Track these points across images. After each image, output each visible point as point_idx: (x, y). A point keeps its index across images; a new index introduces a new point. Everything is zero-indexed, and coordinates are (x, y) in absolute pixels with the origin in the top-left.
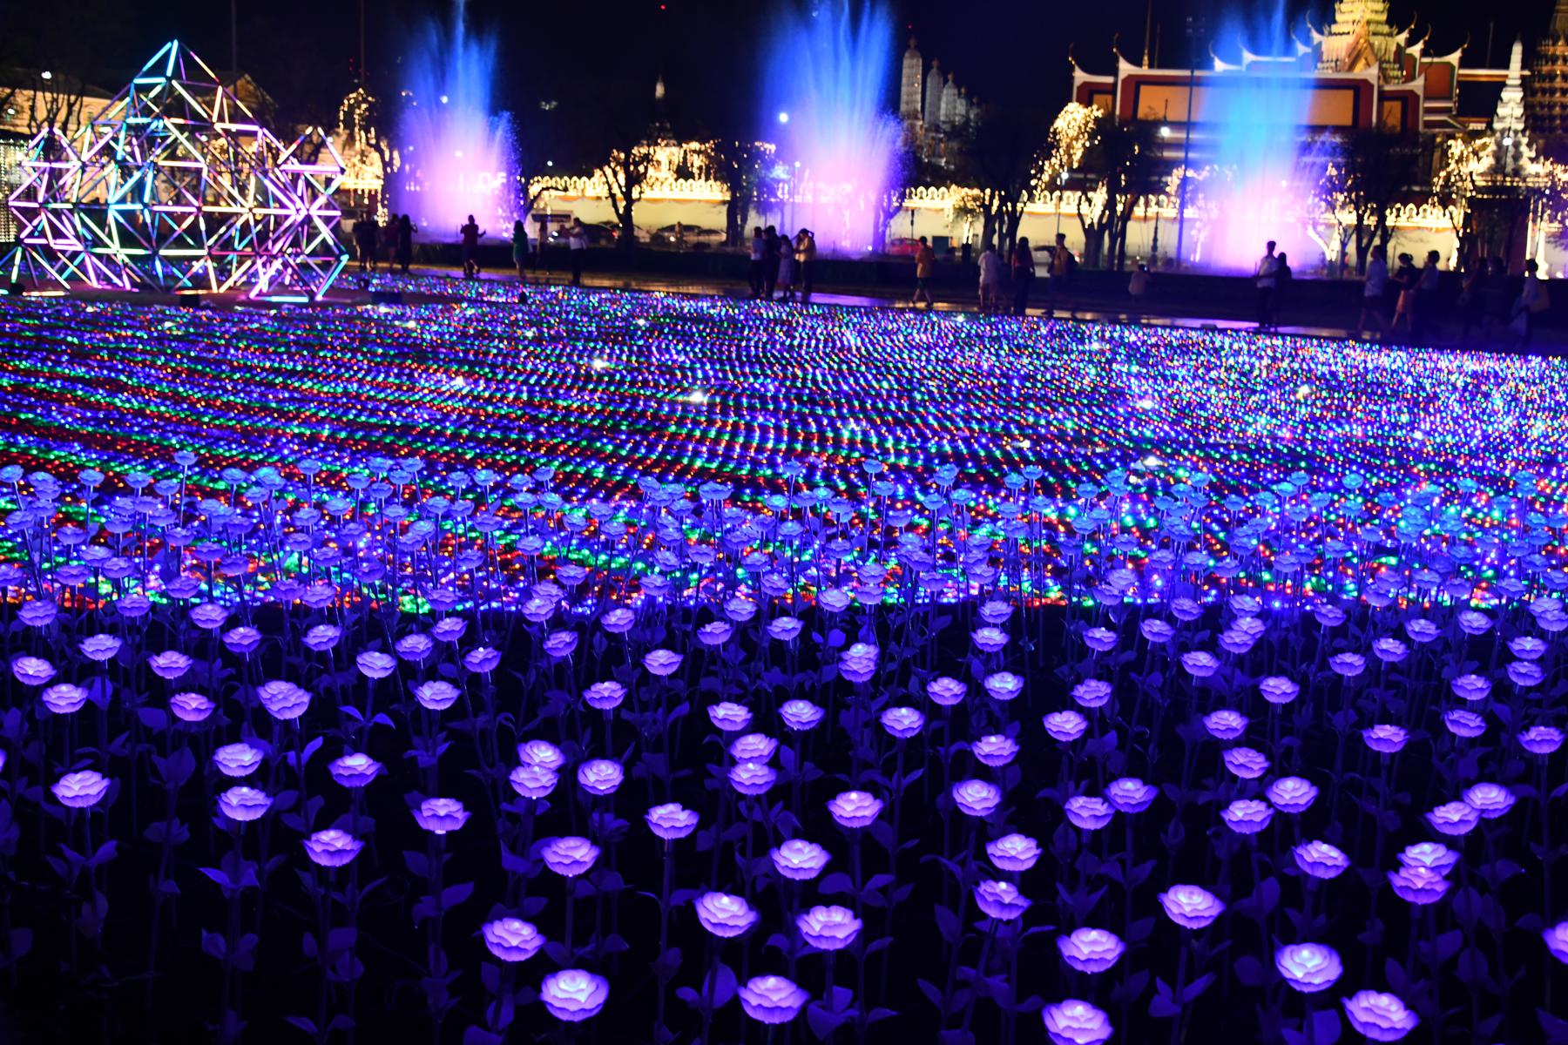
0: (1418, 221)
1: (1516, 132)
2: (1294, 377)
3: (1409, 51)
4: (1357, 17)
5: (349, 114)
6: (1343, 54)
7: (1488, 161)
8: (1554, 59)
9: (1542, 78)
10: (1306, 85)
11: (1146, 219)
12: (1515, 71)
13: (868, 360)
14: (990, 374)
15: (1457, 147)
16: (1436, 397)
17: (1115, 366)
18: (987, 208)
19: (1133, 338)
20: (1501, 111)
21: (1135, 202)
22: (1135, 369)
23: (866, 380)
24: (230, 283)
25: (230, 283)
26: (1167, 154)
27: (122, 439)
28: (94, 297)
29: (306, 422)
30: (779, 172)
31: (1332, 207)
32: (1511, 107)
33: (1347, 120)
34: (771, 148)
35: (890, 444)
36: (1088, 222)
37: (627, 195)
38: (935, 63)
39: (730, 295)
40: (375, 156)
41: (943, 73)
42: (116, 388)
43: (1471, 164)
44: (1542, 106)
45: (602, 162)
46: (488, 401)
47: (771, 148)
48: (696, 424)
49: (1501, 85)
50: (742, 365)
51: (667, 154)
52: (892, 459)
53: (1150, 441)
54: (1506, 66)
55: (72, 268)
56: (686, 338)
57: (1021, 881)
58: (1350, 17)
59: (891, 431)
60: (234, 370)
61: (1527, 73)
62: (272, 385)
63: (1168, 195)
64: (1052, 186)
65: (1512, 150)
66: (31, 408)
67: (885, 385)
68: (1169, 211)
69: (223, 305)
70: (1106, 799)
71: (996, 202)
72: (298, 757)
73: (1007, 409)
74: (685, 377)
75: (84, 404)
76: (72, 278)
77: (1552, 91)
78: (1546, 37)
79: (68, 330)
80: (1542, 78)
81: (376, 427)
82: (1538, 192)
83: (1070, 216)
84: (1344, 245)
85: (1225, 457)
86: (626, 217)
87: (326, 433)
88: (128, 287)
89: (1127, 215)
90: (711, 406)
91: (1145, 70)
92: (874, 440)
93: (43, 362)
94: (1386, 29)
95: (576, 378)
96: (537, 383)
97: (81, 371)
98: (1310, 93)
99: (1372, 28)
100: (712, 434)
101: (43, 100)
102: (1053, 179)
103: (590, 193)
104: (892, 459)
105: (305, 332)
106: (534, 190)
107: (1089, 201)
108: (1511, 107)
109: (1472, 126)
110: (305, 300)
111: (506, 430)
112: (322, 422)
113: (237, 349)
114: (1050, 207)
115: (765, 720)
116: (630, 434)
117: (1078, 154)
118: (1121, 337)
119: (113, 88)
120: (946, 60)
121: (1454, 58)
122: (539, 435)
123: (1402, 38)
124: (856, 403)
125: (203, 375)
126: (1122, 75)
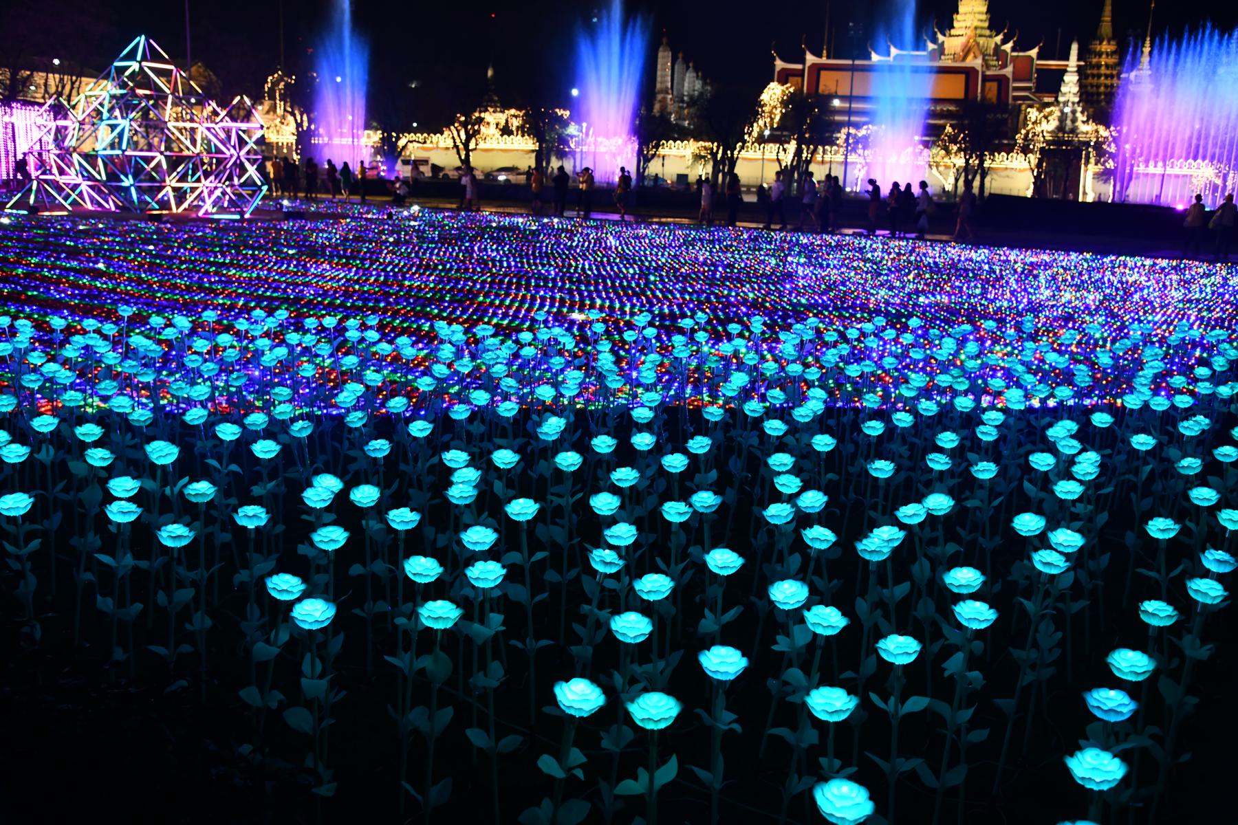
0: (1007, 164)
1: (1073, 103)
3: (1003, 47)
4: (968, 24)
5: (272, 90)
6: (959, 50)
7: (1053, 124)
8: (1100, 54)
9: (1092, 67)
11: (823, 162)
12: (1073, 62)
13: (622, 256)
14: (704, 264)
15: (1033, 114)
16: (1002, 277)
17: (789, 259)
18: (714, 155)
19: (805, 241)
20: (1063, 89)
21: (814, 152)
22: (802, 260)
23: (619, 268)
24: (185, 205)
25: (185, 205)
26: (838, 118)
27: (98, 308)
28: (87, 215)
29: (228, 296)
30: (572, 129)
31: (948, 152)
32: (1070, 86)
34: (566, 114)
35: (627, 309)
36: (784, 164)
37: (466, 145)
38: (680, 55)
39: (538, 214)
40: (290, 118)
43: (1042, 124)
44: (1092, 86)
45: (449, 123)
46: (356, 282)
49: (1063, 72)
50: (535, 258)
51: (493, 118)
52: (628, 318)
53: (803, 305)
54: (1068, 59)
55: (74, 196)
56: (499, 241)
58: (964, 24)
59: (630, 300)
60: (182, 263)
61: (1082, 63)
62: (207, 273)
63: (838, 145)
64: (761, 140)
65: (1070, 115)
66: (36, 288)
67: (631, 271)
69: (179, 221)
71: (720, 151)
72: (172, 491)
74: (494, 266)
75: (74, 286)
78: (1095, 39)
80: (1092, 67)
81: (277, 299)
82: (1087, 144)
83: (772, 160)
84: (957, 180)
86: (466, 161)
87: (241, 303)
88: (113, 209)
91: (824, 60)
92: (617, 305)
93: (48, 258)
94: (988, 32)
95: (419, 267)
96: (392, 270)
98: (934, 76)
99: (978, 32)
100: (507, 302)
101: (53, 80)
102: (761, 135)
103: (442, 145)
104: (628, 318)
105: (233, 239)
106: (401, 143)
107: (785, 150)
108: (1070, 86)
109: (1046, 100)
110: (237, 217)
111: (366, 300)
112: (239, 296)
113: (185, 249)
114: (758, 155)
115: (481, 460)
116: (450, 302)
117: (777, 118)
118: (797, 240)
119: (100, 71)
121: (1033, 53)
122: (388, 303)
123: (999, 39)
124: (609, 282)
125: (160, 265)
126: (808, 64)
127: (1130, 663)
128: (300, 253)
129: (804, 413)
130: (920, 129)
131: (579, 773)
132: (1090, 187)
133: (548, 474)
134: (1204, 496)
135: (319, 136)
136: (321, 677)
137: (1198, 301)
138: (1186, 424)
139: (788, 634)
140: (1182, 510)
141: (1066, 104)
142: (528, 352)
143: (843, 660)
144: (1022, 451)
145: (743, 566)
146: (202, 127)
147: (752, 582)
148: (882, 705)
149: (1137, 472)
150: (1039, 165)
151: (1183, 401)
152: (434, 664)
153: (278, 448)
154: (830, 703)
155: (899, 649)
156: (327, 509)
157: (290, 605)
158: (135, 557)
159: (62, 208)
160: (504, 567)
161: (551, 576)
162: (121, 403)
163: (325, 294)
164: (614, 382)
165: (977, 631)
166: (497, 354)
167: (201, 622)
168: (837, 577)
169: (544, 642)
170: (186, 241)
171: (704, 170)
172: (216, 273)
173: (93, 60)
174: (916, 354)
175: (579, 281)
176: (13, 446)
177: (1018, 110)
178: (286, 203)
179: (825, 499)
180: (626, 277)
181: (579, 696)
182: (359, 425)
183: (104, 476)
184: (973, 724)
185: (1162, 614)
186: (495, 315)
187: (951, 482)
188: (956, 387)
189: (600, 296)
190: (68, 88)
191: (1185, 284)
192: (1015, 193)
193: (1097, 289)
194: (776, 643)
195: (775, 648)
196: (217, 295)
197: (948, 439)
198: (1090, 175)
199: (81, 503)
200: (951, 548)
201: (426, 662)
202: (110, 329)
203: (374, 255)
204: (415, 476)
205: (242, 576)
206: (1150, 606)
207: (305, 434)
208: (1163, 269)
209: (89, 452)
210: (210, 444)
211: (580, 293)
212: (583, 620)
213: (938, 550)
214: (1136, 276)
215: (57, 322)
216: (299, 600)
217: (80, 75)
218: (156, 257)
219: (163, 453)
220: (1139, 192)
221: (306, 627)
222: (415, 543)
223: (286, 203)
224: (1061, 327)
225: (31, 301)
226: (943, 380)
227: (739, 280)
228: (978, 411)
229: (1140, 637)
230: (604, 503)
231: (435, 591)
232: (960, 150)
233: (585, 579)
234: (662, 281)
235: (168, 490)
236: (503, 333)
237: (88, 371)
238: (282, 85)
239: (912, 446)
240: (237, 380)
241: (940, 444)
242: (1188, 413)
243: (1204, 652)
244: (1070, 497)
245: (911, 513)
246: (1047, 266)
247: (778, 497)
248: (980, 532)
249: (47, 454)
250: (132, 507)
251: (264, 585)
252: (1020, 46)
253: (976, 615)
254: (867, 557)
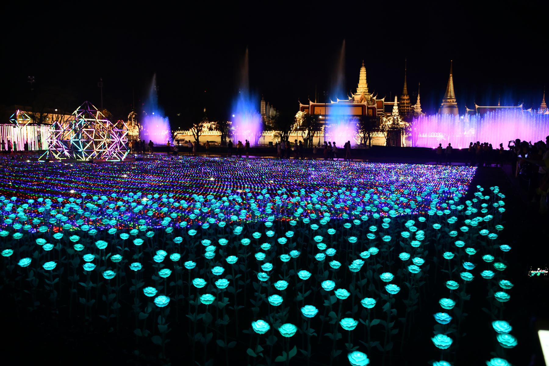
5: (130, 117)
6: (359, 99)
7: (391, 122)
8: (404, 100)
9: (402, 104)
12: (396, 102)
13: (253, 170)
14: (281, 171)
15: (384, 119)
18: (281, 135)
21: (314, 133)
22: (313, 169)
29: (118, 188)
30: (233, 128)
31: (358, 133)
32: (396, 110)
33: (361, 114)
35: (256, 188)
37: (197, 134)
39: (223, 156)
40: (137, 127)
41: (270, 105)
43: (388, 123)
45: (191, 127)
46: (162, 182)
48: (211, 185)
49: (392, 106)
51: (206, 125)
56: (210, 166)
59: (257, 185)
60: (101, 177)
62: (110, 180)
64: (296, 130)
66: (50, 187)
68: (322, 135)
70: (289, 255)
75: (63, 186)
77: (404, 107)
80: (402, 104)
81: (135, 188)
82: (402, 128)
85: (332, 187)
86: (197, 140)
89: (313, 136)
90: (215, 181)
91: (316, 104)
92: (253, 187)
95: (183, 176)
97: (63, 179)
101: (55, 116)
102: (296, 128)
103: (189, 134)
106: (175, 134)
108: (396, 110)
111: (166, 188)
112: (121, 188)
114: (296, 135)
115: (215, 243)
116: (195, 188)
117: (301, 123)
120: (270, 102)
121: (383, 100)
122: (174, 189)
127: (447, 303)
128: (142, 172)
129: (324, 221)
130: (434, 119)
131: (261, 354)
133: (237, 246)
134: (460, 244)
138: (450, 219)
140: (453, 249)
141: (395, 116)
142: (227, 204)
144: (398, 230)
145: (311, 276)
147: (315, 282)
148: (364, 323)
149: (436, 236)
151: (447, 212)
153: (143, 241)
154: (348, 323)
155: (369, 303)
157: (153, 298)
158: (93, 283)
161: (241, 283)
162: (85, 227)
163: (152, 186)
164: (258, 214)
166: (216, 205)
167: (117, 306)
168: (343, 278)
169: (240, 307)
170: (102, 170)
171: (278, 140)
172: (113, 180)
174: (358, 200)
175: (239, 179)
177: (379, 118)
178: (136, 155)
179: (335, 251)
180: (254, 177)
181: (261, 326)
182: (170, 232)
183: (80, 255)
184: (394, 328)
185: (454, 285)
186: (211, 191)
187: (376, 243)
188: (373, 210)
189: (246, 184)
190: (60, 119)
191: (439, 173)
192: (380, 145)
193: (411, 175)
194: (324, 303)
195: (324, 304)
197: (373, 228)
198: (404, 138)
199: (70, 264)
200: (379, 266)
202: (79, 201)
203: (167, 173)
204: (192, 249)
205: (133, 288)
206: (450, 283)
207: (151, 236)
212: (255, 298)
213: (374, 267)
214: (423, 171)
215: (60, 200)
217: (64, 114)
219: (102, 245)
220: (420, 144)
221: (160, 306)
222: (195, 274)
223: (136, 155)
224: (401, 188)
225: (48, 192)
226: (368, 208)
227: (293, 177)
228: (382, 218)
229: (448, 294)
230: (260, 256)
231: (204, 291)
232: (361, 131)
233: (254, 283)
236: (218, 198)
237: (72, 216)
238: (134, 116)
239: (361, 231)
242: (449, 216)
243: (468, 298)
244: (416, 246)
245: (365, 254)
246: (394, 168)
248: (388, 259)
250: (93, 265)
253: (393, 289)
254: (353, 271)
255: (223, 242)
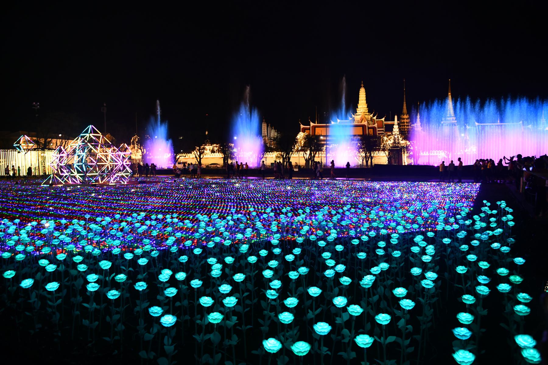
2: (352, 189)
5: (133, 141)
6: (359, 119)
7: (392, 141)
8: (404, 119)
9: (402, 123)
10: (351, 126)
12: (396, 122)
14: (283, 191)
15: (385, 138)
18: (283, 156)
20: (394, 130)
21: (316, 153)
22: (316, 189)
29: (121, 210)
30: (235, 150)
31: (359, 152)
32: (396, 129)
33: (361, 133)
34: (233, 145)
35: (260, 208)
37: (200, 156)
39: (225, 178)
40: (140, 151)
41: (271, 127)
42: (75, 205)
43: (389, 142)
45: (194, 149)
46: (165, 203)
47: (233, 145)
51: (208, 147)
57: (277, 290)
59: (260, 205)
60: (104, 200)
62: (113, 203)
64: (298, 151)
69: (102, 186)
73: (287, 199)
75: (66, 209)
76: (65, 182)
77: (404, 126)
79: (64, 193)
80: (402, 123)
82: (404, 147)
86: (200, 162)
89: (314, 157)
91: (316, 124)
92: (256, 207)
95: (186, 198)
97: (66, 202)
98: (352, 128)
101: (59, 141)
103: (191, 157)
106: (178, 157)
108: (396, 129)
111: (169, 209)
112: (125, 210)
114: (297, 155)
115: (221, 261)
116: (199, 209)
121: (383, 119)
122: (177, 210)
123: (372, 115)
126: (311, 125)
128: (145, 195)
132: (406, 160)
133: (243, 265)
134: (472, 257)
135: (150, 156)
136: (172, 345)
137: (448, 195)
138: (459, 234)
139: (340, 316)
142: (231, 223)
143: (364, 324)
146: (109, 156)
148: (379, 340)
150: (389, 155)
151: (456, 227)
152: (214, 337)
155: (383, 319)
156: (166, 282)
158: (97, 305)
159: (61, 183)
160: (236, 298)
162: (89, 248)
164: (263, 232)
165: (409, 310)
166: (221, 224)
168: (354, 294)
169: (249, 327)
172: (116, 203)
173: (71, 134)
175: (242, 200)
176: (51, 265)
177: (380, 138)
181: (272, 345)
182: (175, 251)
184: (410, 345)
185: (471, 299)
196: (117, 210)
197: (382, 244)
198: (405, 157)
201: (211, 336)
202: (82, 222)
203: (170, 195)
206: (466, 297)
207: (156, 255)
208: (434, 185)
209: (79, 266)
210: (121, 261)
211: (243, 203)
216: (403, 298)
218: (95, 198)
219: (106, 265)
220: (422, 162)
222: (201, 292)
226: (375, 224)
229: (465, 308)
230: (268, 274)
234: (270, 198)
235: (107, 278)
236: (222, 218)
237: (75, 237)
240: (130, 238)
241: (379, 246)
242: (458, 231)
243: (485, 312)
245: (376, 270)
246: (397, 186)
247: (328, 268)
248: (400, 274)
249: (62, 268)
250: (96, 285)
251: (148, 311)
252: (379, 117)
253: (407, 304)
254: (364, 286)
255: (229, 260)
